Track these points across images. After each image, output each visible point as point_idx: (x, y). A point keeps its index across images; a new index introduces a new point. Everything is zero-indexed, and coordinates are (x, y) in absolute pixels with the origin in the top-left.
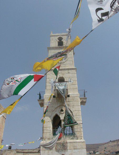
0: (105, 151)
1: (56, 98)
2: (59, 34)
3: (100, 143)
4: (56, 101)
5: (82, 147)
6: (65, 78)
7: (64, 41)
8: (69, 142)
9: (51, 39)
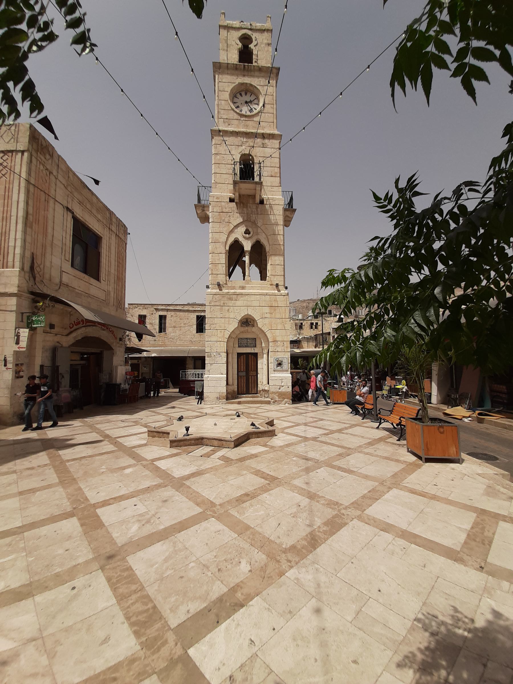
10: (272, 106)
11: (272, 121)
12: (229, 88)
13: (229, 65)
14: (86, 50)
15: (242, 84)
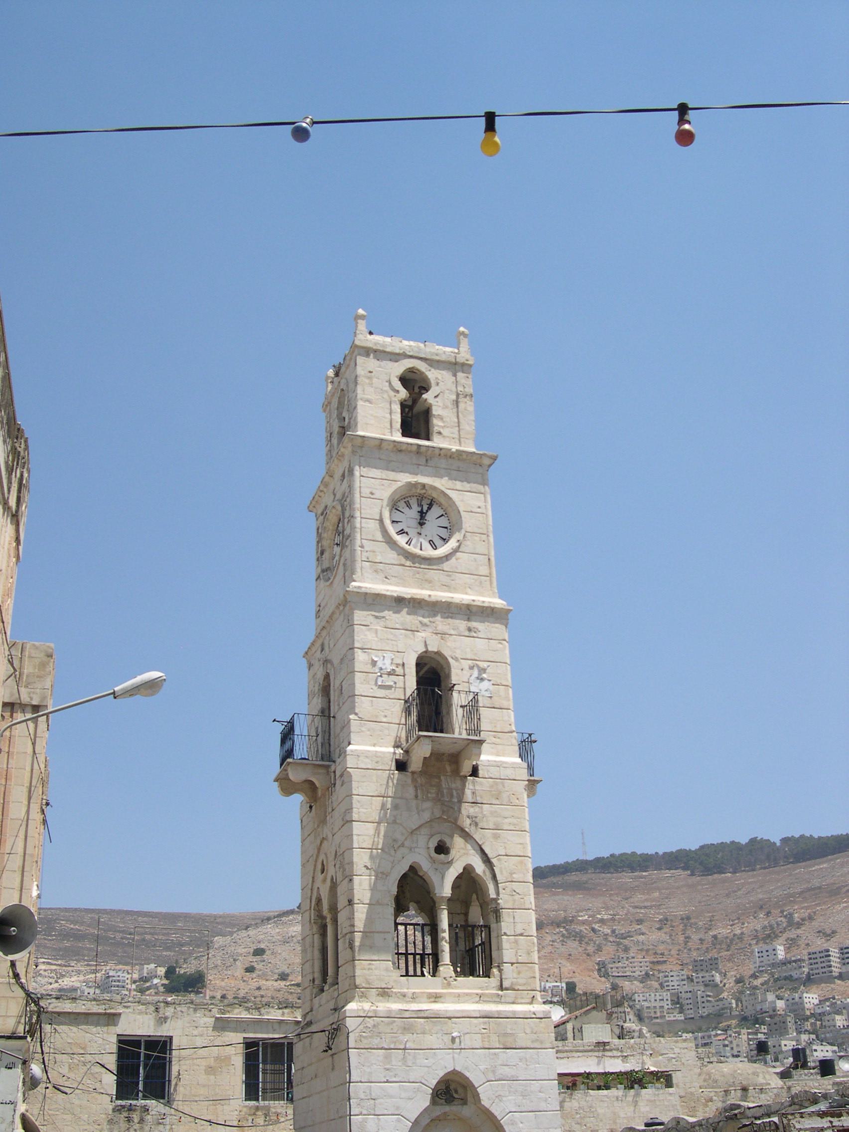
0: (250, 969)
1: (413, 773)
2: (407, 345)
3: (215, 912)
4: (411, 791)
5: (537, 1040)
6: (450, 660)
7: (439, 399)
8: (483, 1014)
9: (360, 371)
10: (484, 537)
11: (486, 572)
12: (386, 492)
13: (384, 444)
14: (456, 886)
15: (416, 485)
